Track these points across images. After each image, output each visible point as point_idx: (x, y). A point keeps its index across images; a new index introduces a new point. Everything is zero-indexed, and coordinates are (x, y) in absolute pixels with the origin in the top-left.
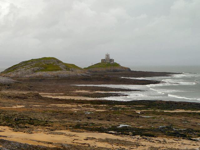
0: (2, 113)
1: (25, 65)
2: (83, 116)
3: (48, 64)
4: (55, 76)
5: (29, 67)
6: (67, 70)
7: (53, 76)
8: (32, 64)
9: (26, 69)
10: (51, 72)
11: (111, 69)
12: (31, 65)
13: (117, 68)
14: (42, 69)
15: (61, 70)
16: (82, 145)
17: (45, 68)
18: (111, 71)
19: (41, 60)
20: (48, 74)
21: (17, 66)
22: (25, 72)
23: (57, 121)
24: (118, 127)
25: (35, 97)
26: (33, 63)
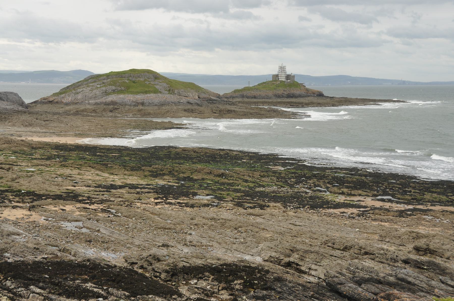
1: (95, 82)
2: (298, 243)
3: (134, 82)
4: (138, 103)
5: (98, 86)
6: (169, 93)
7: (134, 102)
8: (105, 81)
12: (103, 83)
14: (122, 90)
15: (156, 92)
17: (126, 89)
18: (283, 97)
19: (124, 74)
20: (127, 98)
21: (80, 83)
22: (91, 95)
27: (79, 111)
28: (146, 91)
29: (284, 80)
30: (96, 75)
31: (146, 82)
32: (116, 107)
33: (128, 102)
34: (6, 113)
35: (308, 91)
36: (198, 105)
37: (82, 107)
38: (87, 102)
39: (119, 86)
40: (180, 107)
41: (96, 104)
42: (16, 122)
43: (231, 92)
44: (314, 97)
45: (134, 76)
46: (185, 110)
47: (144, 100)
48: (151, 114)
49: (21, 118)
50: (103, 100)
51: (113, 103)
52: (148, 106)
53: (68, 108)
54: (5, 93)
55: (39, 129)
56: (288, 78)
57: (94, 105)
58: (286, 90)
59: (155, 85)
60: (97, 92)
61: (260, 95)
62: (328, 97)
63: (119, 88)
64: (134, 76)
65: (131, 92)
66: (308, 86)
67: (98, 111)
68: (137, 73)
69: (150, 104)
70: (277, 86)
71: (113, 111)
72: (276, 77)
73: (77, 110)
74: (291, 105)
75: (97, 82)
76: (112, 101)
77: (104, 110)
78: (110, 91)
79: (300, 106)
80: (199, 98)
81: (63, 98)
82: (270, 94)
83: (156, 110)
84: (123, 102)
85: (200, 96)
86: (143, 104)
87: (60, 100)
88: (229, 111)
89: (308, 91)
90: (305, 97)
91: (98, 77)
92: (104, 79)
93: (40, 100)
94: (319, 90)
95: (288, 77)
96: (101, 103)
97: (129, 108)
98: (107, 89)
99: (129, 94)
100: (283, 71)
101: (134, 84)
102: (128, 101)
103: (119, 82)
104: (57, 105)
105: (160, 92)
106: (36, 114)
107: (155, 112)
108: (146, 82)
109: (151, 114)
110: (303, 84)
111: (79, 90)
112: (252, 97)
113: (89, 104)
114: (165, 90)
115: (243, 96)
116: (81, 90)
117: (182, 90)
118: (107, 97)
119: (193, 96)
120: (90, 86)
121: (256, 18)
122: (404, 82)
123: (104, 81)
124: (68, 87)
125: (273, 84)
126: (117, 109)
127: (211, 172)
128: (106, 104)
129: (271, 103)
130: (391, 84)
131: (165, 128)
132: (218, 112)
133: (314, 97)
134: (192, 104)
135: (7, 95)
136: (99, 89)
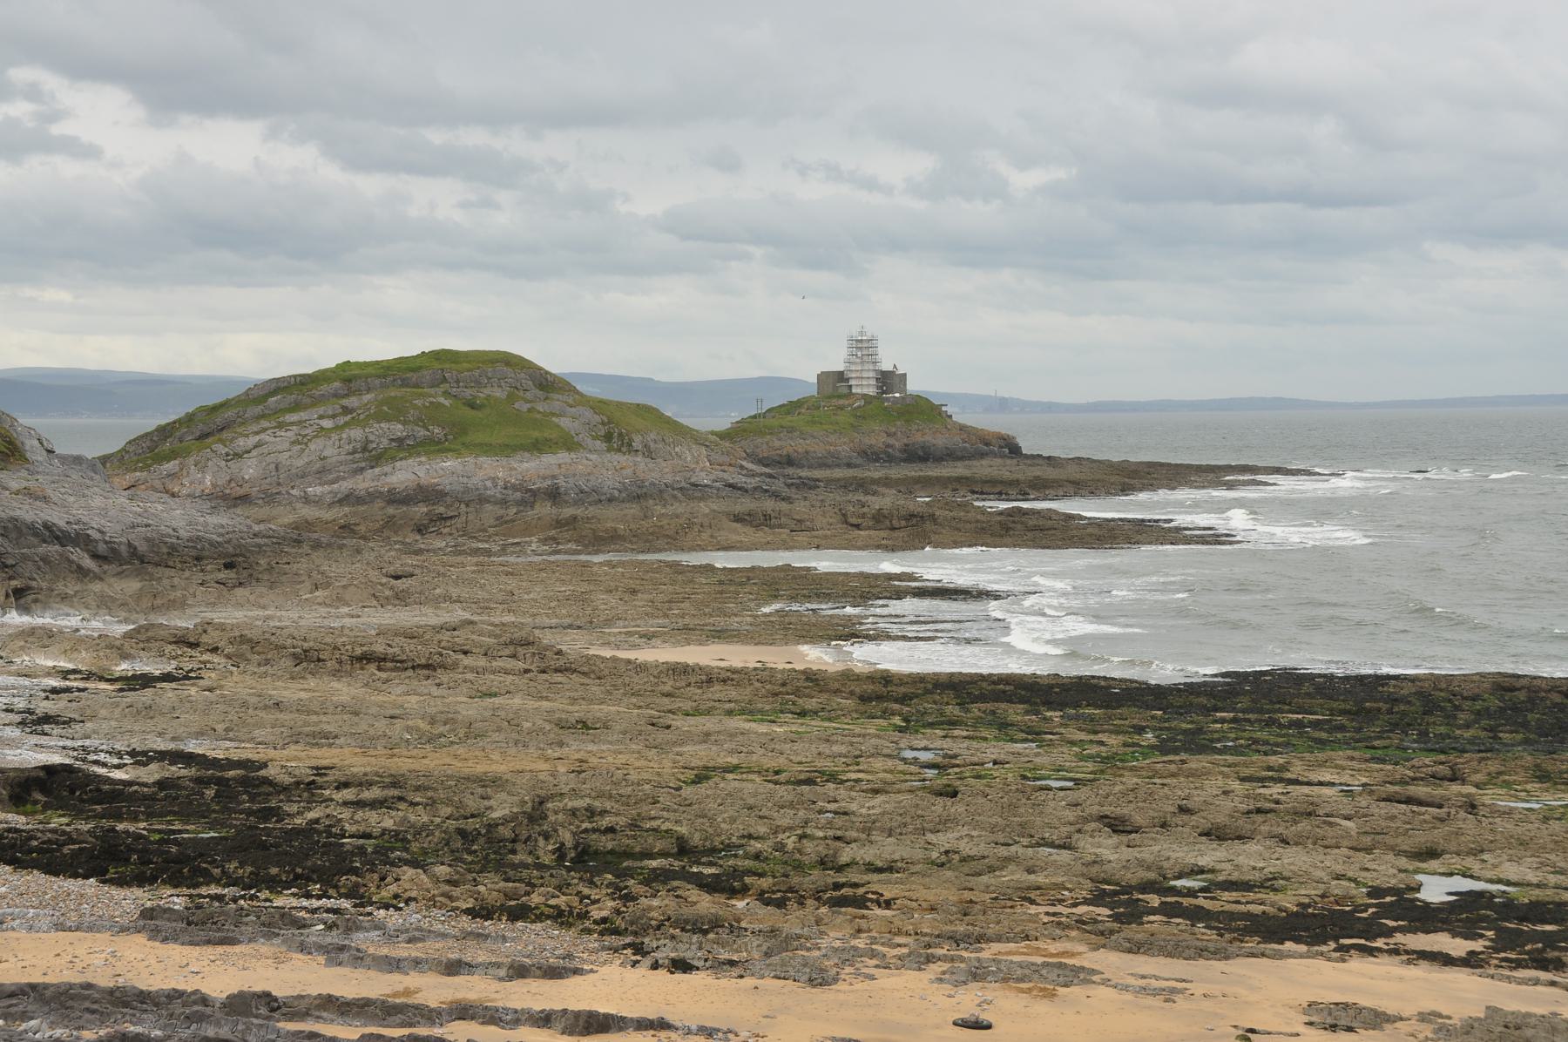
0: (401, 799)
1: (296, 407)
4: (534, 493)
5: (327, 423)
6: (609, 450)
7: (515, 488)
8: (352, 402)
10: (504, 461)
11: (891, 441)
12: (346, 410)
13: (927, 438)
15: (569, 444)
18: (890, 459)
20: (481, 474)
21: (229, 414)
22: (300, 463)
24: (1477, 946)
25: (514, 656)
26: (358, 392)
31: (516, 406)
32: (441, 510)
33: (486, 489)
34: (259, 546)
39: (419, 421)
41: (348, 499)
42: (344, 587)
44: (1001, 457)
45: (458, 381)
46: (738, 519)
47: (554, 477)
50: (364, 483)
55: (460, 612)
56: (884, 384)
58: (894, 430)
59: (553, 414)
61: (807, 452)
63: (422, 433)
65: (481, 445)
66: (961, 417)
67: (362, 529)
71: (426, 527)
72: (835, 382)
74: (973, 492)
76: (420, 488)
77: (390, 524)
78: (385, 443)
82: (844, 448)
84: (467, 490)
86: (554, 495)
88: (912, 516)
90: (969, 458)
91: (302, 384)
94: (1003, 432)
95: (888, 380)
96: (371, 497)
97: (501, 512)
98: (372, 438)
100: (865, 358)
101: (479, 414)
102: (489, 484)
103: (415, 407)
107: (632, 526)
108: (516, 406)
110: (944, 409)
111: (242, 443)
113: (307, 500)
114: (595, 438)
116: (253, 440)
118: (387, 469)
123: (345, 402)
124: (164, 432)
125: (841, 408)
126: (446, 519)
128: (395, 498)
136: (334, 437)
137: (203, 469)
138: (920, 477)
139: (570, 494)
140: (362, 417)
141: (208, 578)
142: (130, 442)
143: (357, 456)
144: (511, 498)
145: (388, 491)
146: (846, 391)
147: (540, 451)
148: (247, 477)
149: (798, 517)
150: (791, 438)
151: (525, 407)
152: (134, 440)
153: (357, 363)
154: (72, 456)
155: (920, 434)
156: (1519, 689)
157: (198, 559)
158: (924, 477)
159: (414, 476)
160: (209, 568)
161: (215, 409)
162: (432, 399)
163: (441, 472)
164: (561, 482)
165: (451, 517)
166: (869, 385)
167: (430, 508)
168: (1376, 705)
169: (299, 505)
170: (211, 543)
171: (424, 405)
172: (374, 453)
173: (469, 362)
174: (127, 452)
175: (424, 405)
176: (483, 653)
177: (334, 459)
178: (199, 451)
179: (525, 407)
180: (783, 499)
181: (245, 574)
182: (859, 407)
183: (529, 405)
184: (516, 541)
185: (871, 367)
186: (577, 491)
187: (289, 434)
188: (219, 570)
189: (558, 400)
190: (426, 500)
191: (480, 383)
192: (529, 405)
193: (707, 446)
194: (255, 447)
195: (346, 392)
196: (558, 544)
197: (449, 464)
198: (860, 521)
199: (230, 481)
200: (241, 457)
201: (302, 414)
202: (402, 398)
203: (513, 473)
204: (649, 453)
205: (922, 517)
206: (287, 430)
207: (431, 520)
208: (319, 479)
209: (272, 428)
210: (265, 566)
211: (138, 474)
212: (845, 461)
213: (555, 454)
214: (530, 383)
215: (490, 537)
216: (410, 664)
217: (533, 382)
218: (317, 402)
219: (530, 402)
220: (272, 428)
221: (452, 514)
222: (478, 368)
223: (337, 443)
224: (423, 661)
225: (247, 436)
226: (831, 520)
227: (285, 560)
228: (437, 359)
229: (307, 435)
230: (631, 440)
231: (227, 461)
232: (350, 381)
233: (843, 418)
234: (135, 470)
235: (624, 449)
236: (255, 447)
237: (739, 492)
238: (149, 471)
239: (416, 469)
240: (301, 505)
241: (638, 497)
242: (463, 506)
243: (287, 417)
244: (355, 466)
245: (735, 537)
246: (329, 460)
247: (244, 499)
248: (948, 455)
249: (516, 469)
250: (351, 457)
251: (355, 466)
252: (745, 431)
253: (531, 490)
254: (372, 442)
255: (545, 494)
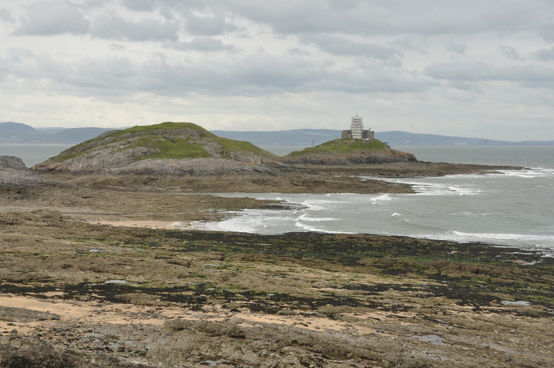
1: (114, 141)
3: (173, 141)
4: (185, 172)
5: (122, 147)
6: (222, 157)
7: (178, 170)
8: (131, 140)
9: (112, 153)
11: (363, 156)
12: (129, 142)
15: (205, 155)
16: (519, 320)
19: (157, 129)
20: (168, 165)
21: (92, 143)
22: (111, 160)
23: (214, 257)
25: (44, 221)
27: (99, 183)
28: (192, 154)
29: (360, 138)
30: (115, 131)
32: (152, 177)
33: (169, 170)
34: (33, 186)
35: (394, 154)
36: (270, 174)
37: (102, 178)
38: (107, 170)
39: (153, 147)
40: (245, 177)
41: (121, 173)
42: (53, 200)
43: (288, 156)
44: (404, 162)
45: (171, 133)
46: (254, 182)
47: (192, 166)
48: (208, 187)
49: (55, 194)
50: (133, 166)
51: (148, 171)
52: (199, 175)
53: (79, 179)
54: (4, 158)
56: (365, 135)
57: (120, 174)
58: (365, 151)
59: (202, 145)
60: (121, 156)
61: (329, 159)
62: (422, 162)
63: (153, 150)
64: (171, 133)
66: (394, 146)
67: (126, 183)
68: (174, 128)
69: (202, 173)
70: (351, 147)
71: (147, 183)
73: (95, 181)
75: (118, 141)
77: (135, 181)
79: (394, 175)
80: (262, 163)
81: (69, 164)
82: (343, 157)
83: (214, 180)
84: (162, 170)
85: (264, 161)
86: (191, 172)
87: (65, 167)
88: (316, 182)
89: (394, 154)
90: (392, 162)
92: (128, 137)
93: (34, 168)
95: (365, 134)
96: (130, 172)
97: (172, 178)
98: (136, 152)
99: (169, 159)
100: (358, 126)
101: (175, 144)
102: (170, 168)
103: (152, 142)
104: (61, 175)
105: (210, 156)
106: (70, 188)
107: (213, 183)
109: (208, 187)
110: (387, 144)
112: (318, 163)
113: (110, 173)
114: (217, 153)
115: (306, 162)
116: (97, 152)
117: (239, 153)
118: (138, 163)
119: (254, 162)
120: (110, 147)
121: (230, 49)
122: (486, 142)
123: (129, 140)
124: (73, 149)
125: (346, 143)
127: (460, 268)
128: (138, 173)
129: (350, 171)
130: (467, 144)
131: (260, 207)
132: (301, 184)
133: (405, 162)
134: (261, 172)
135: (7, 162)
136: (123, 151)
137: (79, 161)
138: (363, 168)
139: (197, 172)
140: (134, 145)
141: (11, 196)
142: (62, 153)
143: (130, 158)
144: (176, 173)
145: (136, 170)
146: (350, 137)
147: (193, 157)
148: (93, 165)
149: (275, 182)
150: (324, 154)
151: (192, 142)
152: (63, 152)
153: (140, 126)
154: (11, 156)
155: (374, 153)
156: (355, 238)
157: (8, 190)
158: (364, 169)
159: (146, 165)
160: (12, 193)
161: (89, 141)
162: (158, 139)
163: (155, 164)
164: (194, 168)
165: (156, 179)
166: (358, 135)
167: (149, 176)
168: (294, 241)
169: (107, 174)
170: (15, 185)
171: (155, 141)
172: (136, 157)
173: (176, 126)
174: (61, 156)
175: (155, 141)
176: (35, 220)
177: (122, 159)
178: (79, 156)
179: (192, 142)
180: (273, 175)
181: (24, 195)
182: (353, 143)
183: (194, 142)
184: (172, 187)
185: (359, 129)
186: (199, 171)
187: (109, 150)
188: (15, 194)
189: (205, 140)
190: (148, 173)
191: (179, 134)
192: (194, 142)
193: (267, 156)
194: (97, 155)
195: (132, 136)
196: (186, 189)
197: (158, 161)
198: (297, 183)
199: (88, 166)
200: (92, 158)
201: (114, 144)
202: (148, 139)
203: (179, 164)
204: (237, 159)
205: (320, 182)
206: (108, 149)
207: (149, 180)
208: (117, 165)
209: (103, 148)
210: (32, 193)
211: (58, 163)
212: (343, 163)
213: (198, 158)
214: (197, 134)
215: (165, 186)
216: (6, 223)
217: (198, 133)
218: (121, 139)
219: (194, 140)
220: (103, 148)
221: (156, 178)
222: (179, 129)
223: (124, 154)
224: (10, 222)
225: (95, 151)
226: (287, 183)
227: (41, 191)
228: (165, 125)
229: (115, 151)
230: (230, 154)
231: (87, 159)
232: (134, 132)
233: (346, 147)
234: (58, 162)
235: (227, 157)
236: (97, 155)
237: (258, 172)
238: (62, 162)
239: (147, 163)
240: (108, 174)
241: (220, 174)
242: (160, 176)
243: (109, 144)
244: (129, 161)
245: (250, 188)
246: (121, 160)
247: (91, 172)
248: (384, 161)
249: (180, 163)
250: (128, 158)
251: (129, 161)
252: (307, 151)
253: (184, 171)
254: (135, 153)
255: (188, 172)
